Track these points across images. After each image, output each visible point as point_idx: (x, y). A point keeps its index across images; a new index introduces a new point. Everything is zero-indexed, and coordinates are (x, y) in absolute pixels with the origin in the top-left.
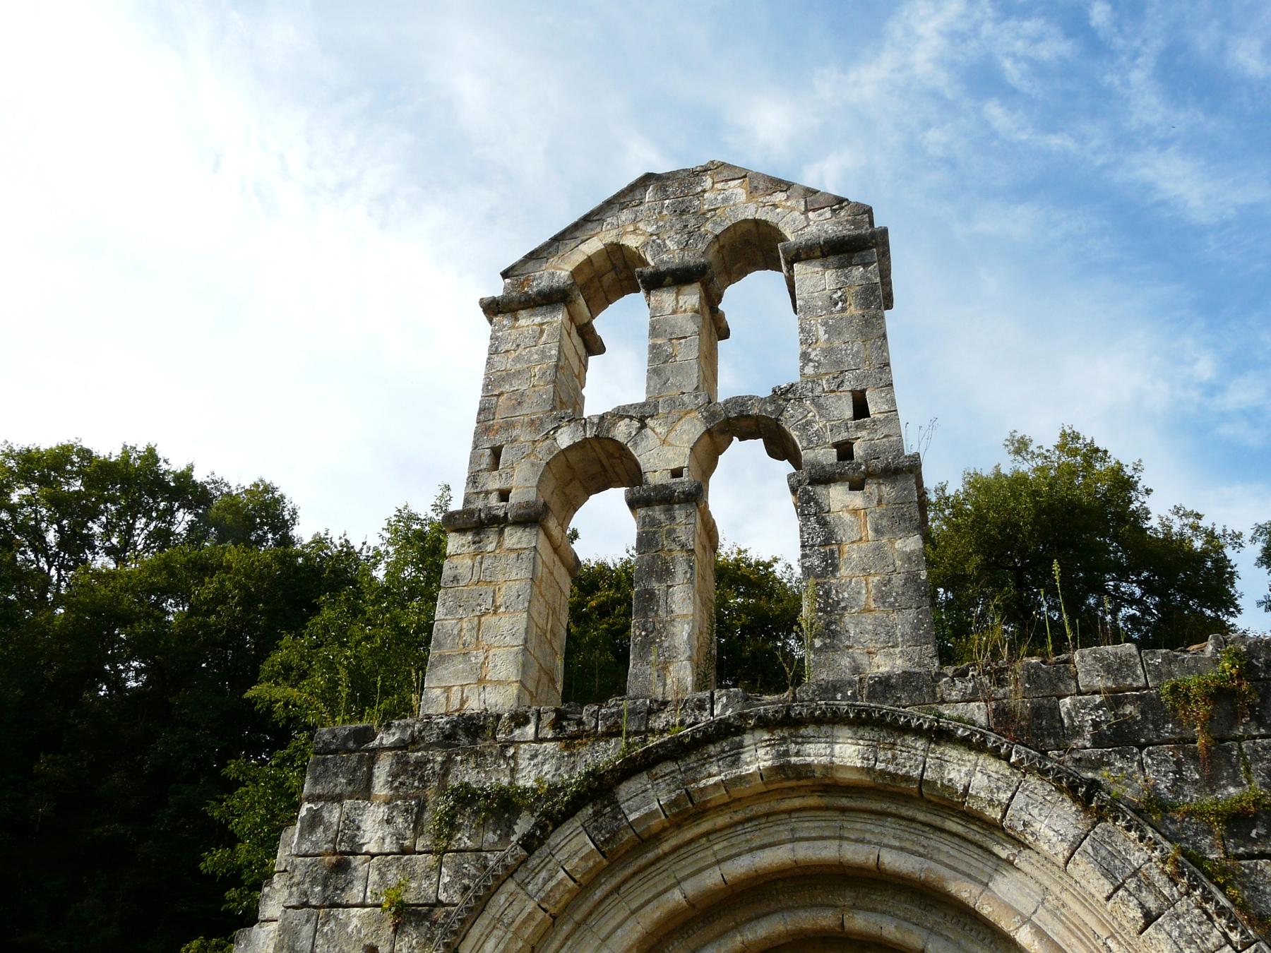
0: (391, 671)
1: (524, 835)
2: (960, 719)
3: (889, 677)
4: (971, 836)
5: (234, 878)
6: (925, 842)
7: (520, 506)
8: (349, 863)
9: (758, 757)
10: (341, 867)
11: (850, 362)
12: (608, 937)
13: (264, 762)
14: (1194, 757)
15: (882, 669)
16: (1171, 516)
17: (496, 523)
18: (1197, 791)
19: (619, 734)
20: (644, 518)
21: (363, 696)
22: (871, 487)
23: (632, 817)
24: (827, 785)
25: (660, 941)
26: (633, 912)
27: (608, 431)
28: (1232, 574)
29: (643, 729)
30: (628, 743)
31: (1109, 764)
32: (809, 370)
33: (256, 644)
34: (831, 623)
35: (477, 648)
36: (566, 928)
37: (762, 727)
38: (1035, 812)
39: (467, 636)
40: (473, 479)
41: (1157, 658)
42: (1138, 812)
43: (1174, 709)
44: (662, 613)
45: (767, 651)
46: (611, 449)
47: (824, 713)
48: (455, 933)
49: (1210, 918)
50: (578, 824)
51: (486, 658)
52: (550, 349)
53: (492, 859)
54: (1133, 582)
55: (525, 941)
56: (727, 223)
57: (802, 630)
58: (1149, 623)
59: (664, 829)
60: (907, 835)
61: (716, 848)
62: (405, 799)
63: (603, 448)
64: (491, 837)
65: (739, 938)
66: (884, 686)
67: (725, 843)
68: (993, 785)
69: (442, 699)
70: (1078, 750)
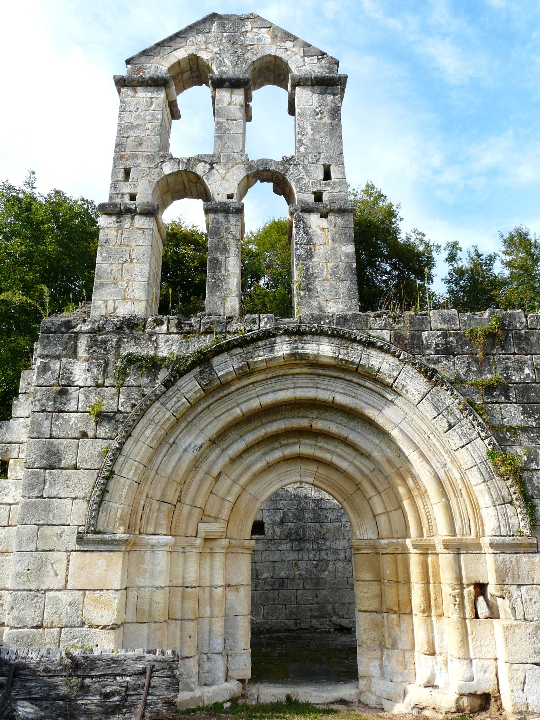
2: (378, 338)
4: (376, 390)
6: (356, 391)
7: (144, 204)
9: (283, 348)
10: (63, 392)
11: (323, 148)
12: (203, 429)
14: (476, 361)
16: (411, 234)
17: (131, 212)
18: (475, 375)
19: (212, 332)
20: (213, 219)
22: (331, 217)
23: (220, 374)
25: (225, 431)
26: (216, 418)
27: (192, 168)
32: (302, 149)
34: (309, 284)
36: (184, 425)
38: (408, 381)
40: (114, 185)
41: (466, 316)
42: (451, 383)
43: (470, 340)
46: (192, 177)
48: (130, 426)
49: (474, 427)
52: (157, 114)
53: (147, 391)
56: (260, 55)
59: (233, 380)
61: (257, 389)
62: (97, 359)
63: (188, 177)
64: (145, 380)
65: (263, 430)
67: (262, 388)
69: (103, 306)
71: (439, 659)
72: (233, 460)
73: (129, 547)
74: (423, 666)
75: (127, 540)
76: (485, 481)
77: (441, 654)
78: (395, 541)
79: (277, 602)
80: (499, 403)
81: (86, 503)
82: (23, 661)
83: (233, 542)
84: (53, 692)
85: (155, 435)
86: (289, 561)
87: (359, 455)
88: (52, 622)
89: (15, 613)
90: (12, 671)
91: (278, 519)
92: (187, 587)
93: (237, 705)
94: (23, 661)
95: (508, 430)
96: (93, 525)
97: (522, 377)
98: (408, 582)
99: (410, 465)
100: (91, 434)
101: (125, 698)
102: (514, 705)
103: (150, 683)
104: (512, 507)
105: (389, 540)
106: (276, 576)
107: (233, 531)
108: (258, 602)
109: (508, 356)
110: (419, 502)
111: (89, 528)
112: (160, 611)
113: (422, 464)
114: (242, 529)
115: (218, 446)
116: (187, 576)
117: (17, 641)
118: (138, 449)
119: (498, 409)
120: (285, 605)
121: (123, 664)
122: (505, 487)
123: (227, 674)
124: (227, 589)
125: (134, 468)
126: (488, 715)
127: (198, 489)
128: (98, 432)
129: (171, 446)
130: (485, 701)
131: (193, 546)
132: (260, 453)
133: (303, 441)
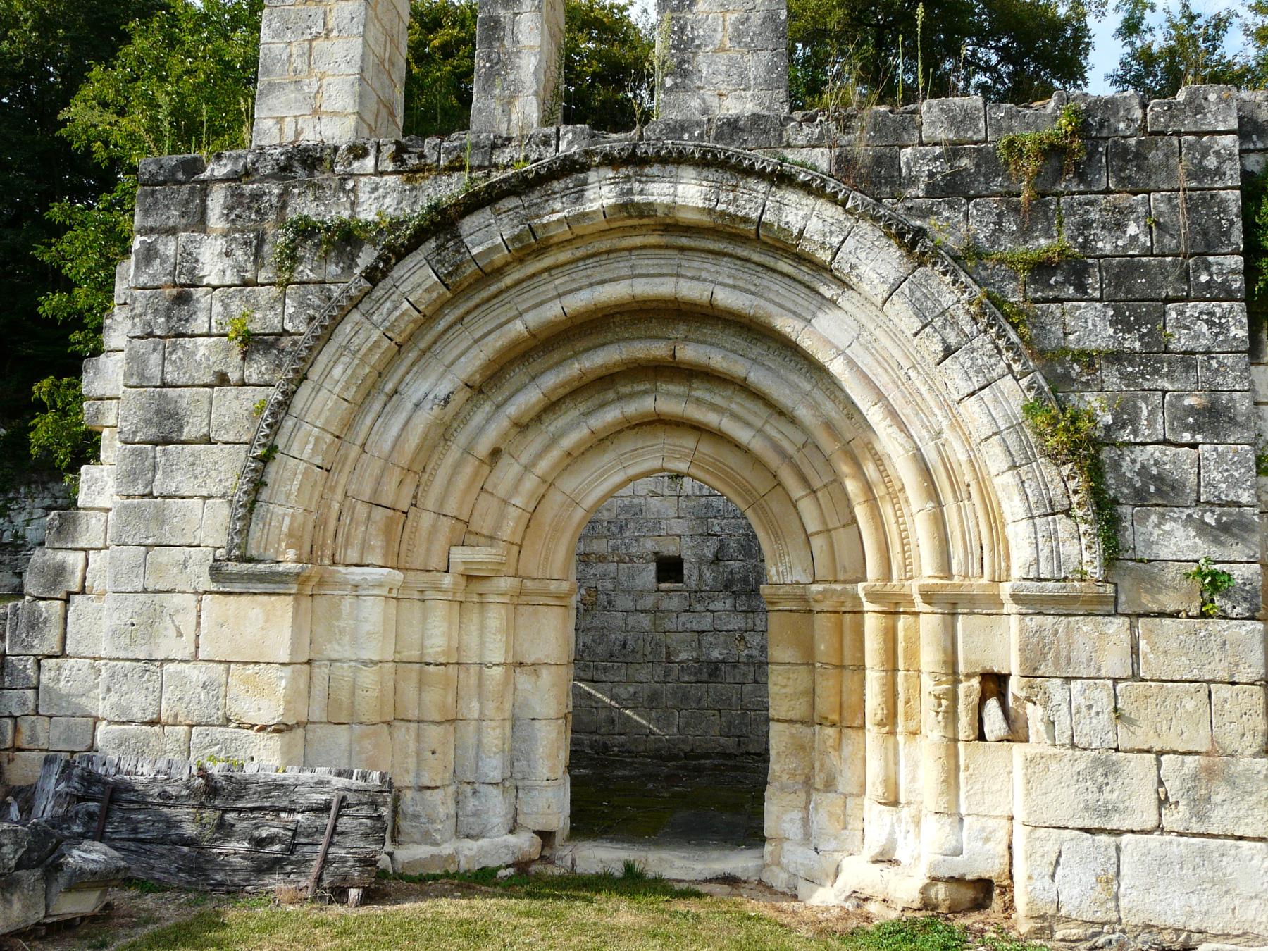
0: (219, 109)
1: (367, 268)
2: (802, 164)
3: (737, 120)
4: (800, 277)
5: (76, 321)
6: (757, 281)
8: (190, 295)
9: (601, 193)
10: (183, 299)
13: (90, 207)
14: (1016, 210)
15: (732, 112)
18: (1012, 241)
19: (461, 168)
21: (188, 129)
23: (475, 252)
24: (668, 225)
25: (502, 368)
26: (476, 342)
28: (1088, 44)
29: (487, 163)
30: (471, 178)
31: (937, 213)
33: (62, 77)
34: (684, 61)
35: (309, 75)
36: (412, 356)
37: (607, 165)
38: (862, 256)
39: (298, 63)
42: (956, 259)
43: (1007, 164)
44: (507, 43)
45: (616, 102)
47: (670, 152)
48: (303, 359)
49: (1000, 352)
50: (422, 257)
51: (320, 87)
53: (336, 291)
54: (992, 48)
55: (373, 367)
57: (653, 69)
58: (998, 92)
59: (507, 264)
60: (741, 274)
61: (557, 282)
62: (243, 231)
64: (334, 269)
65: (577, 366)
66: (732, 127)
67: (566, 278)
68: (827, 230)
69: (275, 130)
70: (911, 198)
71: (905, 812)
72: (522, 427)
73: (309, 586)
74: (876, 822)
75: (298, 574)
76: (1014, 466)
77: (909, 803)
78: (838, 587)
79: (703, 704)
80: (1061, 301)
81: (227, 505)
82: (127, 777)
83: (529, 583)
84: (173, 832)
85: (352, 375)
86: (728, 631)
87: (776, 416)
88: (176, 716)
89: (113, 698)
90: (108, 792)
91: (709, 554)
92: (428, 664)
93: (527, 873)
94: (127, 777)
95: (1075, 359)
96: (238, 546)
97: (1120, 243)
98: (861, 667)
99: (871, 435)
100: (234, 376)
101: (292, 848)
102: (1031, 902)
103: (335, 826)
104: (1070, 522)
105: (828, 586)
106: (703, 658)
107: (531, 564)
108: (670, 703)
109: (1092, 197)
110: (887, 510)
111: (230, 551)
112: (368, 705)
113: (889, 430)
114: (546, 558)
115: (488, 397)
116: (428, 643)
117: (120, 745)
118: (320, 404)
119: (1058, 313)
120: (719, 710)
121: (293, 792)
122: (1058, 479)
123: (515, 821)
124: (518, 670)
125: (312, 439)
126: (982, 918)
127: (450, 481)
128: (247, 373)
129: (391, 397)
130: (981, 892)
131: (437, 588)
132: (577, 413)
133: (663, 387)
